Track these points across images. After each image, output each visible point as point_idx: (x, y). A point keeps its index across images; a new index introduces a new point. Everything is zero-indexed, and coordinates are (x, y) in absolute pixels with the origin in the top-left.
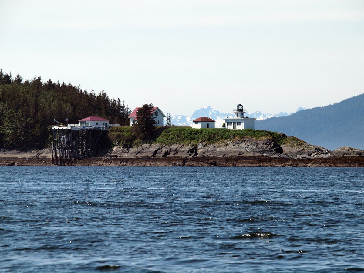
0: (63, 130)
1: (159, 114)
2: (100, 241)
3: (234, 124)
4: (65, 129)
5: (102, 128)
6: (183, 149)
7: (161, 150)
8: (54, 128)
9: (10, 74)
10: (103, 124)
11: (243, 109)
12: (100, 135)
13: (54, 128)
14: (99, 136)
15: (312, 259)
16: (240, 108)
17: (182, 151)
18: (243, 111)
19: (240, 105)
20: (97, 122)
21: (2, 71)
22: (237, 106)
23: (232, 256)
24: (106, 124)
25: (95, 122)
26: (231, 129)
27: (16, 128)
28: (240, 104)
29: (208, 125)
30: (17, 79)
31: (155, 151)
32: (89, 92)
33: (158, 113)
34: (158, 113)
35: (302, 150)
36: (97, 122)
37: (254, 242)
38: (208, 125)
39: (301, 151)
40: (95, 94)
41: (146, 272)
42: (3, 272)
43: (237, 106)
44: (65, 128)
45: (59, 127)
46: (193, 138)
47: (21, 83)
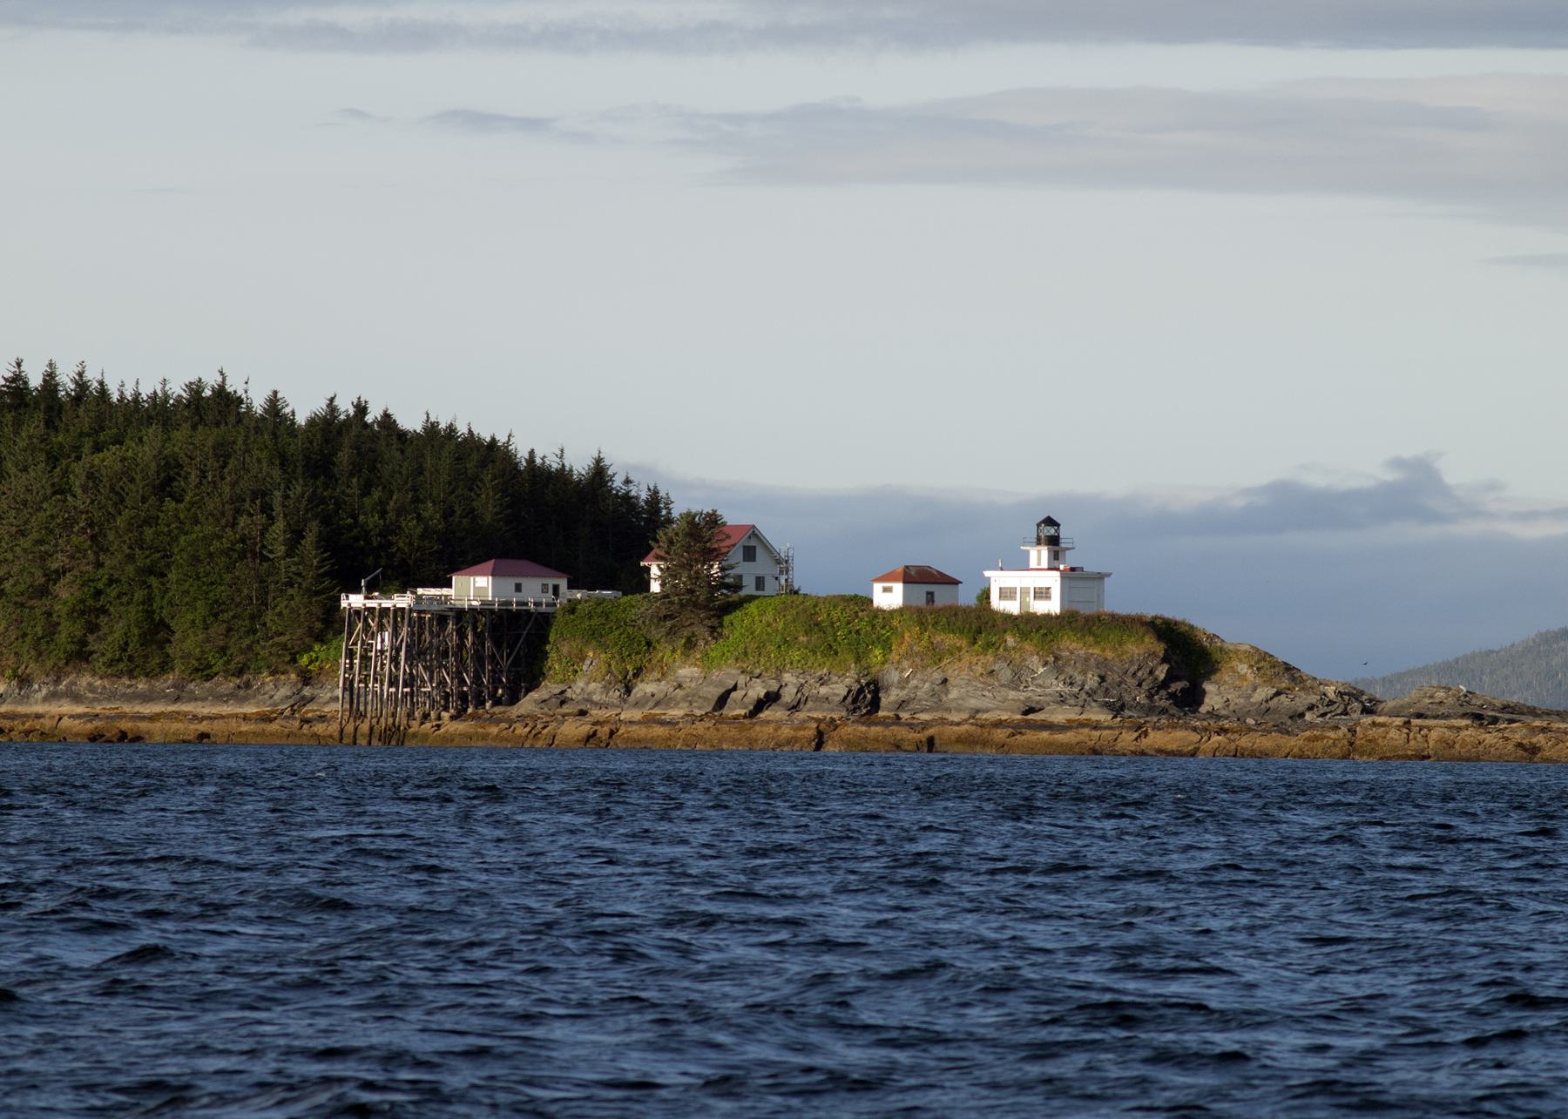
0: (384, 612)
1: (759, 552)
2: (799, 1047)
3: (1024, 595)
4: (389, 609)
5: (535, 604)
6: (823, 690)
7: (743, 692)
9: (246, 392)
10: (545, 587)
12: (525, 632)
14: (520, 635)
17: (823, 697)
18: (1062, 545)
19: (1049, 522)
21: (224, 380)
23: (1056, 1082)
24: (556, 589)
25: (510, 583)
26: (969, 607)
29: (930, 595)
33: (754, 547)
34: (754, 547)
35: (1271, 699)
36: (518, 580)
37: (105, 1006)
38: (930, 595)
40: (293, 413)
44: (387, 604)
46: (158, 503)
47: (171, 402)
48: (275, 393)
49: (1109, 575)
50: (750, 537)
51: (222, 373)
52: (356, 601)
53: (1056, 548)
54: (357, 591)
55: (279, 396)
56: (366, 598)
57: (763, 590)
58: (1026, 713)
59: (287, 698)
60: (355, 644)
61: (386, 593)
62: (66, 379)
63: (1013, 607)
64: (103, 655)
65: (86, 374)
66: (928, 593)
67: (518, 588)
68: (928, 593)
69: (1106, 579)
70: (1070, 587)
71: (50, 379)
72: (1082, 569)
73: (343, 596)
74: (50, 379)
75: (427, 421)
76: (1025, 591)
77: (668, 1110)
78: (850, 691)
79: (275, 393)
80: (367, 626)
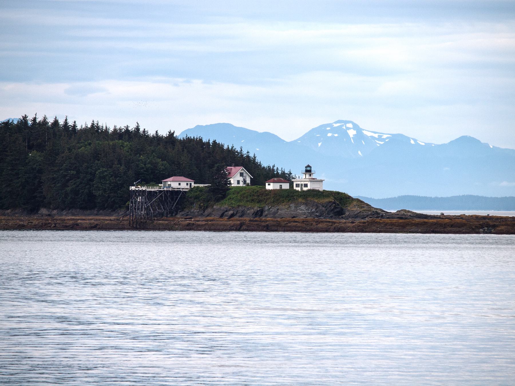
8: (132, 189)
10: (187, 184)
11: (312, 170)
13: (132, 189)
15: (235, 365)
16: (308, 169)
19: (308, 166)
20: (179, 182)
22: (306, 167)
24: (191, 184)
27: (261, 215)
28: (308, 165)
30: (278, 173)
31: (222, 214)
32: (50, 121)
39: (357, 214)
41: (244, 385)
42: (222, 384)
43: (306, 167)
45: (136, 187)
48: (145, 129)
49: (324, 180)
50: (242, 170)
51: (138, 124)
52: (133, 188)
53: (310, 173)
54: (133, 185)
55: (145, 130)
56: (136, 187)
57: (304, 187)
58: (293, 218)
59: (123, 214)
60: (133, 200)
61: (142, 185)
62: (61, 122)
63: (299, 189)
64: (79, 202)
65: (99, 124)
66: (280, 185)
67: (180, 184)
68: (280, 185)
69: (323, 181)
70: (234, 180)
71: (56, 122)
72: (316, 179)
73: (130, 187)
74: (56, 122)
75: (187, 136)
76: (302, 185)
77: (461, 326)
78: (254, 212)
79: (145, 129)
80: (136, 194)
